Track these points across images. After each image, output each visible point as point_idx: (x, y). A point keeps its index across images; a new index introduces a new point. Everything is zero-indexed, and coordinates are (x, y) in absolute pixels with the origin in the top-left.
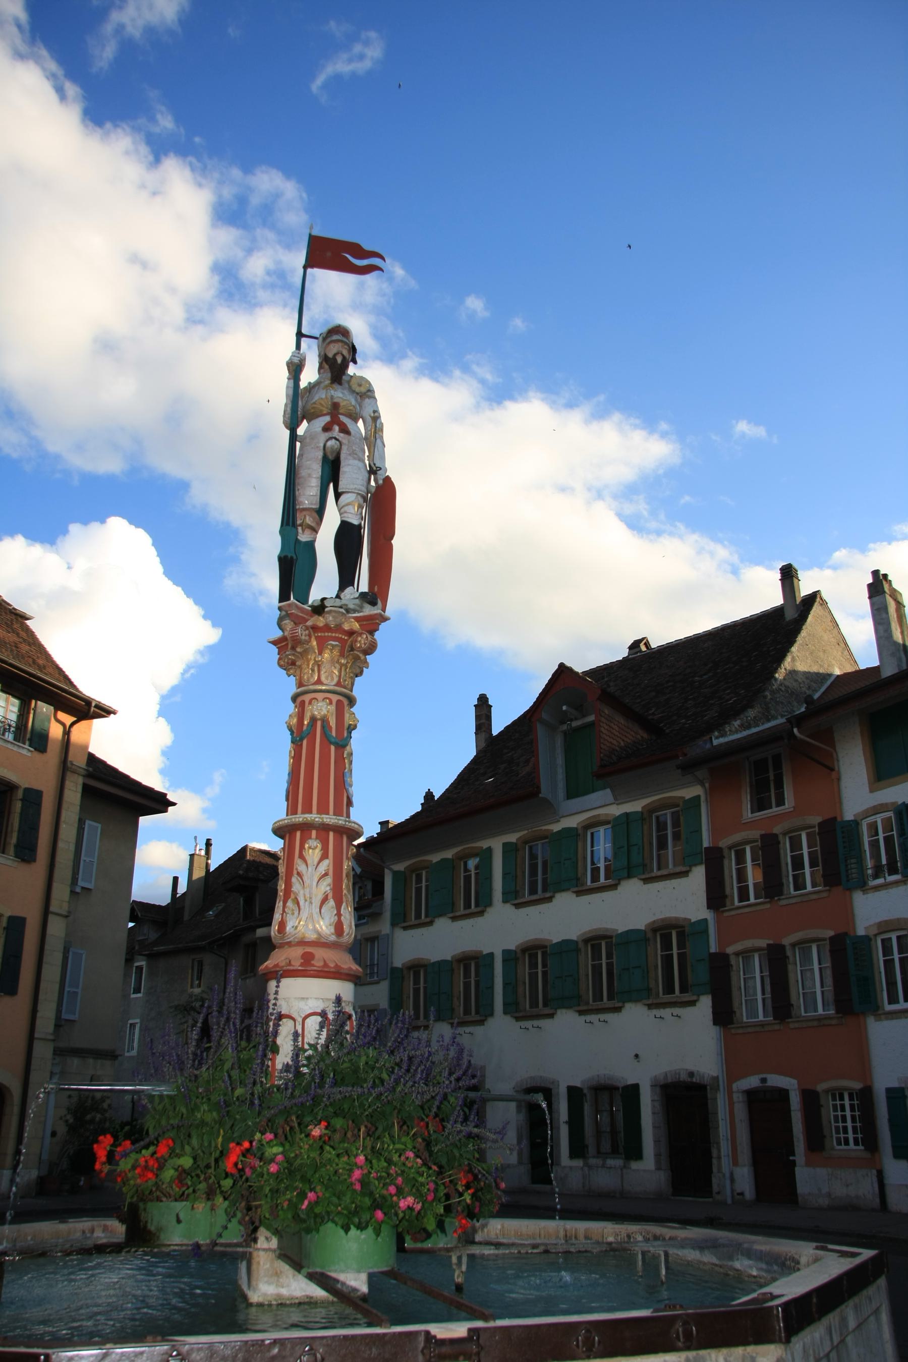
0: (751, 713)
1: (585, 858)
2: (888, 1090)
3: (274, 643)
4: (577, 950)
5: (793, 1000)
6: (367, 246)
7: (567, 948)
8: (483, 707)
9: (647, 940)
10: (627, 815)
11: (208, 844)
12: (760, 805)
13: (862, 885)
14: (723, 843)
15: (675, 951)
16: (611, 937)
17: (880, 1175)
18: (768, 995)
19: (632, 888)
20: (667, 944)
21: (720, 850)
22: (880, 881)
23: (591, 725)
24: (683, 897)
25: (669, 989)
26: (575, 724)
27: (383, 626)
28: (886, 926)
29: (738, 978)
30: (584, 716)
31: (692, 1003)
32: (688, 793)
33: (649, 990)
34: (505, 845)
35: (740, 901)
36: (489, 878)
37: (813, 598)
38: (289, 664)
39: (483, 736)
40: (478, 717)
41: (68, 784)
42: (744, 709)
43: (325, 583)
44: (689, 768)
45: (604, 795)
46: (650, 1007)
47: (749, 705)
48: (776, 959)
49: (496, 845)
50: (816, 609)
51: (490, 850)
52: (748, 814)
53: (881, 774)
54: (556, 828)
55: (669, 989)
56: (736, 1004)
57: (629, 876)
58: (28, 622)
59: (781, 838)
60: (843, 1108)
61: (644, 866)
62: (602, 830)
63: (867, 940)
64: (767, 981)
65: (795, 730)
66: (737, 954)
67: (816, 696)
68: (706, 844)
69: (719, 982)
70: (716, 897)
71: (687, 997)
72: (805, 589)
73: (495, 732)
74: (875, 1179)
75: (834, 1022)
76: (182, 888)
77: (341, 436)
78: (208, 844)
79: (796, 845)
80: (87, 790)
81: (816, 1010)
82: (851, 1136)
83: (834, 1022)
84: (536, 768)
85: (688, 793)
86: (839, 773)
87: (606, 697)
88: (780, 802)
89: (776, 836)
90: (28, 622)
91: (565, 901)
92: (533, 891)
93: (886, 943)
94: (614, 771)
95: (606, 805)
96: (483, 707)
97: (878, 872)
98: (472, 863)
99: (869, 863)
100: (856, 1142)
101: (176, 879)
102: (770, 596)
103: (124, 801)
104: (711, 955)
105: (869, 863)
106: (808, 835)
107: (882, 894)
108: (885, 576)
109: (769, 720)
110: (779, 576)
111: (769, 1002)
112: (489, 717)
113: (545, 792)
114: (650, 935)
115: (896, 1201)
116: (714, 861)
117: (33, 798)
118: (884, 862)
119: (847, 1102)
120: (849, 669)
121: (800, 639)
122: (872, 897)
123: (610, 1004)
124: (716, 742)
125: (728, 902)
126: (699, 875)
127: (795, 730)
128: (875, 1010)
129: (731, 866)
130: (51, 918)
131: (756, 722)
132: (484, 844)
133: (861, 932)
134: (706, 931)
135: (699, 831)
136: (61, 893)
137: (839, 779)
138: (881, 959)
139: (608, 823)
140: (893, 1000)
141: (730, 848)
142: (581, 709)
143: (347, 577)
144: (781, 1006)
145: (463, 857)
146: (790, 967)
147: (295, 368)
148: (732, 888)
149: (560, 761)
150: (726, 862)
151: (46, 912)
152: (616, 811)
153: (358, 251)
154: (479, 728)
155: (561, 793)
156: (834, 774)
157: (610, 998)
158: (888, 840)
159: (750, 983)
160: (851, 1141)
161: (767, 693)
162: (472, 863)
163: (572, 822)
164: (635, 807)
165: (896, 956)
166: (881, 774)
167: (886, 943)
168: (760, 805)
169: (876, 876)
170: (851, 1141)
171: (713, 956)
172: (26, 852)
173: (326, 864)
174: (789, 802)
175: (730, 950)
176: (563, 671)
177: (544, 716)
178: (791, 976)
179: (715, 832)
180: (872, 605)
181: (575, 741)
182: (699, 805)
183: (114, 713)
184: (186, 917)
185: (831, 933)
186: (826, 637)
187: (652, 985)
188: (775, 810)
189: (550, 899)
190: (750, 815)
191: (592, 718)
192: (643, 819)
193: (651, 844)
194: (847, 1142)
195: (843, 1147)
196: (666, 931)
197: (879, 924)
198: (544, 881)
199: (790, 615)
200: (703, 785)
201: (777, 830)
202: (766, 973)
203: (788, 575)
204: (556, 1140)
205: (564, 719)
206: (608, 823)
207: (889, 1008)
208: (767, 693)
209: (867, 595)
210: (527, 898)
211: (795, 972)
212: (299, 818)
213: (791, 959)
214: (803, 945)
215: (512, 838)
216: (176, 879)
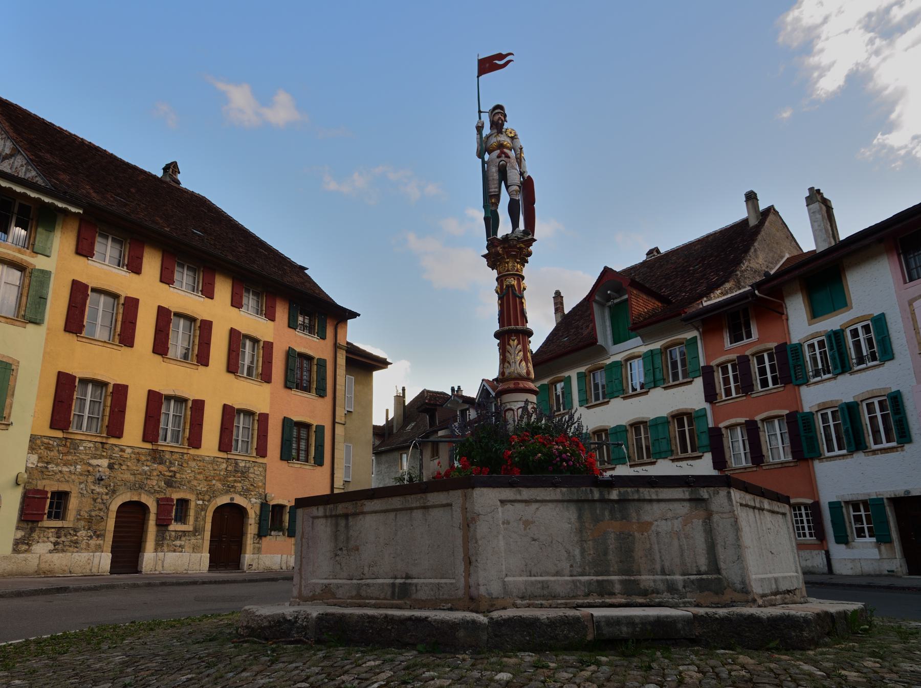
0: (727, 286)
1: (627, 378)
2: (830, 503)
3: (484, 256)
4: (627, 431)
5: (764, 453)
6: (504, 53)
7: (620, 430)
8: (558, 298)
9: (669, 422)
10: (651, 351)
11: (404, 389)
12: (736, 338)
13: (806, 383)
14: (713, 363)
15: (686, 428)
16: (646, 422)
17: (828, 554)
18: (748, 450)
19: (657, 393)
20: (681, 424)
21: (711, 367)
22: (818, 379)
23: (627, 300)
24: (691, 396)
25: (684, 450)
26: (616, 301)
27: (534, 244)
28: (823, 407)
29: (727, 442)
30: (621, 296)
31: (700, 457)
32: (689, 335)
33: (672, 451)
34: (578, 374)
35: (726, 396)
36: (571, 393)
37: (770, 210)
38: (492, 265)
39: (559, 314)
40: (555, 304)
41: (339, 355)
42: (723, 283)
43: (505, 228)
44: (690, 321)
45: (638, 340)
46: (673, 460)
47: (727, 281)
48: (752, 429)
49: (573, 374)
50: (771, 217)
51: (569, 377)
52: (728, 345)
53: (815, 314)
54: (608, 362)
55: (684, 450)
56: (727, 457)
57: (655, 387)
58: (306, 271)
59: (750, 357)
60: (801, 515)
61: (664, 380)
62: (636, 360)
63: (811, 414)
64: (747, 443)
65: (756, 292)
66: (726, 428)
67: (772, 272)
68: (702, 364)
69: (715, 442)
70: (710, 395)
71: (695, 454)
72: (762, 206)
73: (566, 312)
74: (824, 556)
75: (792, 464)
76: (391, 416)
77: (506, 159)
78: (404, 389)
79: (761, 361)
80: (347, 359)
81: (779, 458)
82: (807, 531)
83: (792, 464)
84: (594, 328)
85: (689, 335)
86: (787, 315)
87: (634, 284)
88: (749, 336)
89: (747, 356)
90: (306, 271)
91: (617, 403)
92: (597, 399)
93: (824, 416)
94: (643, 327)
95: (637, 346)
96: (558, 298)
97: (817, 373)
98: (559, 386)
99: (810, 367)
100: (811, 535)
101: (387, 411)
102: (738, 213)
103: (364, 364)
104: (710, 429)
105: (810, 367)
106: (768, 354)
107: (820, 386)
108: (818, 191)
109: (740, 289)
110: (744, 199)
111: (749, 455)
112: (562, 304)
113: (600, 341)
114: (670, 419)
115: (838, 568)
116: (707, 374)
117: (322, 363)
118: (820, 366)
119: (803, 512)
120: (796, 253)
121: (759, 237)
122: (812, 388)
123: (649, 460)
124: (705, 304)
125: (718, 397)
126: (699, 382)
127: (756, 292)
128: (819, 456)
129: (719, 376)
130: (337, 425)
131: (731, 290)
132: (566, 374)
133: (807, 409)
134: (705, 415)
135: (698, 357)
136: (340, 413)
137: (787, 320)
138: (821, 426)
139: (639, 356)
140: (830, 449)
141: (718, 366)
142: (619, 291)
143: (515, 224)
144: (757, 455)
145: (554, 383)
146: (761, 434)
147: (479, 129)
148: (720, 388)
149: (608, 323)
150: (716, 374)
151: (334, 423)
152: (644, 349)
153: (500, 56)
154: (557, 310)
155: (610, 341)
156: (784, 317)
157: (648, 457)
158: (824, 354)
159: (736, 444)
160: (808, 535)
161: (738, 273)
162: (559, 386)
163: (618, 358)
164: (657, 345)
165: (831, 423)
166: (815, 314)
167: (824, 416)
168: (736, 338)
169: (816, 376)
170: (808, 535)
171: (711, 430)
172: (321, 392)
173: (520, 347)
174: (755, 335)
175: (721, 425)
176: (607, 271)
177: (597, 298)
178: (762, 439)
179: (707, 356)
180: (809, 210)
181: (617, 312)
182: (696, 342)
183: (359, 315)
184: (395, 431)
185: (787, 412)
186: (778, 234)
187: (674, 448)
188: (746, 341)
189: (607, 403)
190: (760, 389)
191: (626, 297)
192: (661, 353)
193: (667, 367)
194: (805, 535)
195: (802, 538)
196: (678, 416)
197: (819, 405)
198: (603, 392)
199: (753, 222)
200: (698, 330)
201: (748, 353)
202: (746, 438)
203: (751, 197)
204: (616, 622)
205: (609, 298)
206: (639, 356)
207: (828, 454)
208: (738, 273)
209: (805, 204)
210: (594, 403)
211: (764, 437)
212: (506, 328)
213: (761, 429)
214: (769, 420)
215: (582, 369)
216: (387, 411)
